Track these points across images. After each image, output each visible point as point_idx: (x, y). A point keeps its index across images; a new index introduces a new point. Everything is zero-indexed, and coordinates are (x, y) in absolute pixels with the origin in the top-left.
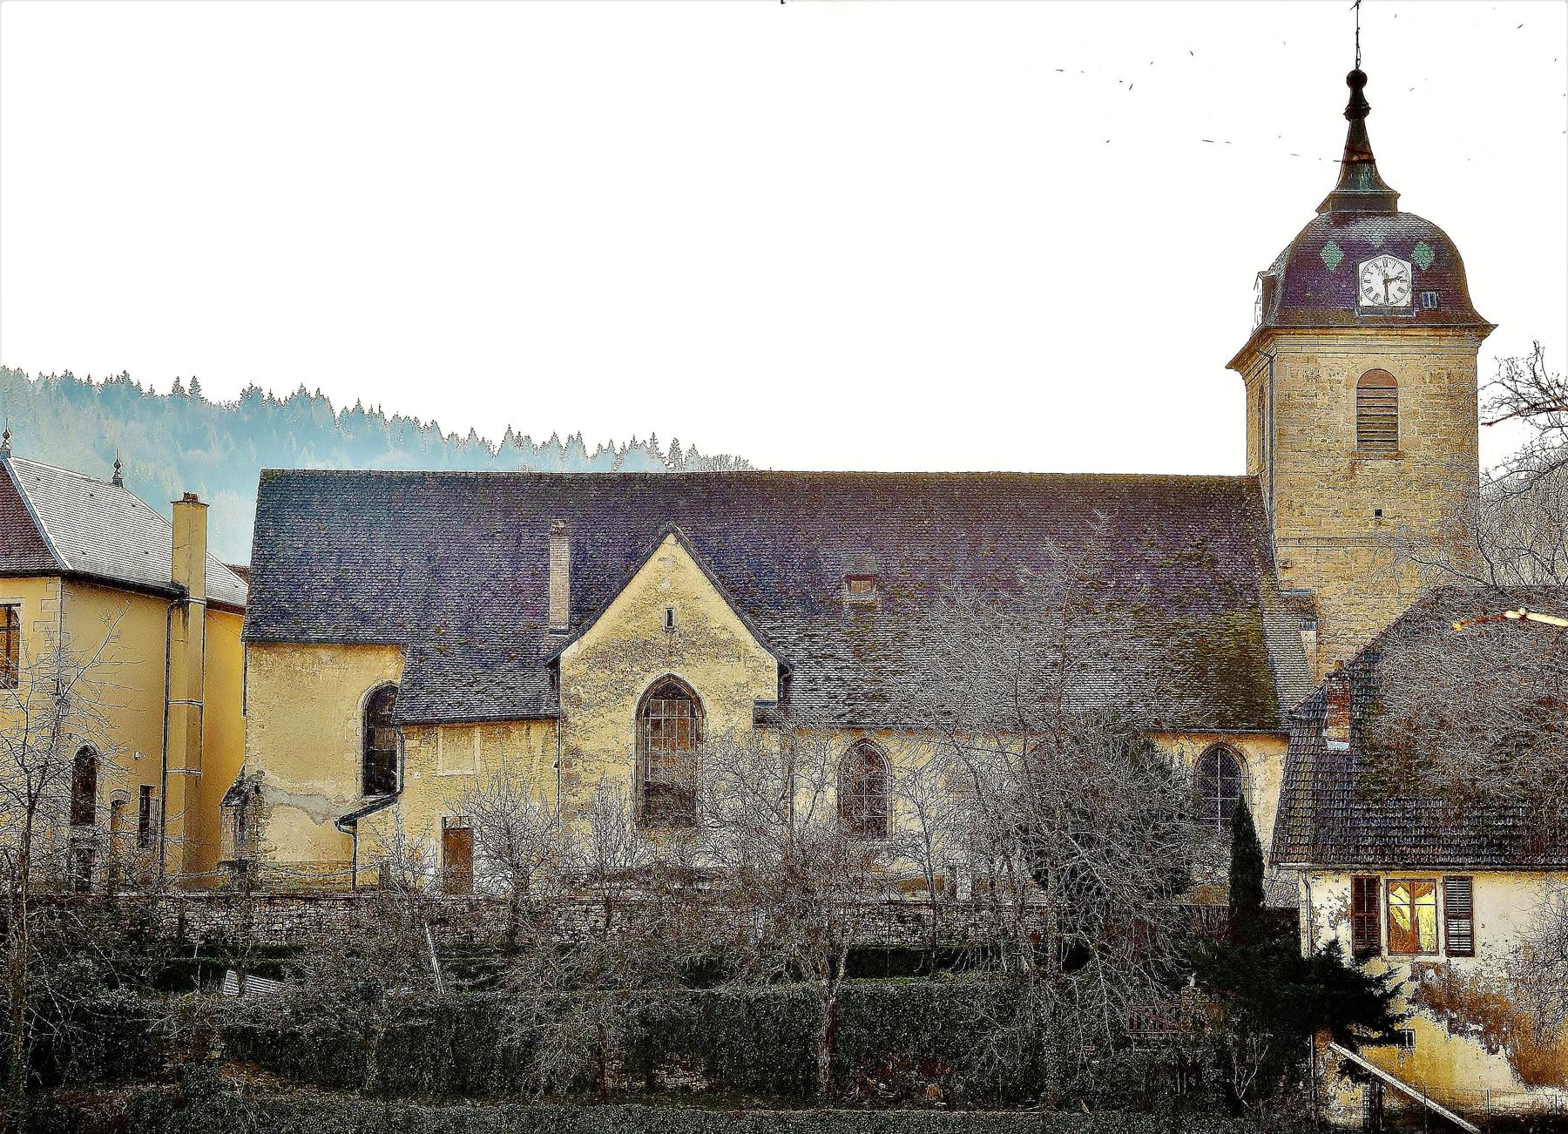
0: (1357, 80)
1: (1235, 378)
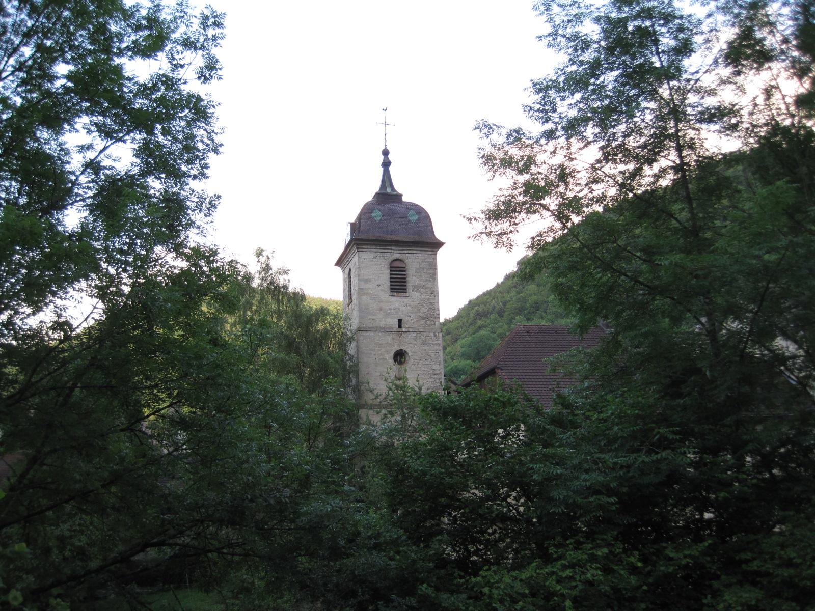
0: (386, 153)
1: (338, 269)
